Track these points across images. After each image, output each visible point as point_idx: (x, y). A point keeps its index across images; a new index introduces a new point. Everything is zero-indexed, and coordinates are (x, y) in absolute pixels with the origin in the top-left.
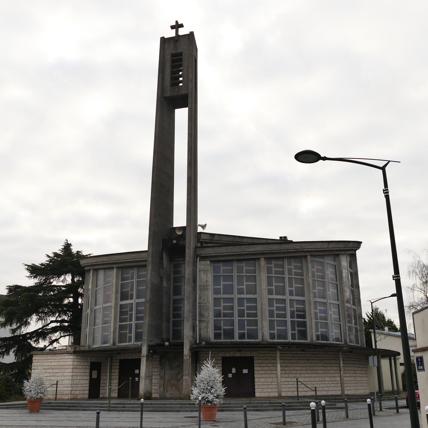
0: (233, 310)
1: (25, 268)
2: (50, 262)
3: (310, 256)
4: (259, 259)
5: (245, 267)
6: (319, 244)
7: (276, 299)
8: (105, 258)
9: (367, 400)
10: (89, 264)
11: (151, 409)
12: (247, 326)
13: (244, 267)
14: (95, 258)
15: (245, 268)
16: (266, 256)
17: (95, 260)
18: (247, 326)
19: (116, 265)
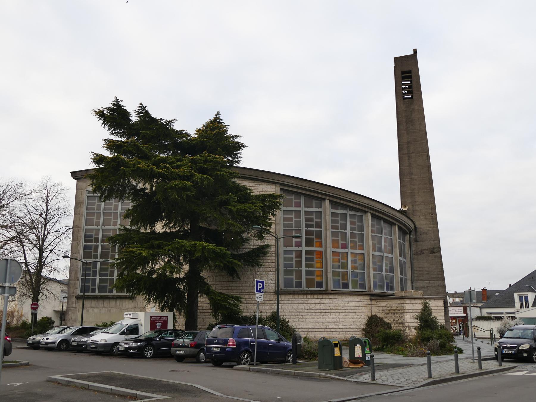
0: (302, 258)
1: (134, 110)
2: (207, 125)
3: (329, 201)
4: (324, 199)
5: (295, 200)
6: (347, 193)
7: (104, 217)
8: (398, 214)
9: (478, 292)
10: (369, 206)
11: (294, 371)
12: (90, 273)
13: (293, 199)
14: (383, 206)
15: (294, 201)
16: (332, 199)
17: (388, 209)
18: (90, 273)
19: (324, 197)
